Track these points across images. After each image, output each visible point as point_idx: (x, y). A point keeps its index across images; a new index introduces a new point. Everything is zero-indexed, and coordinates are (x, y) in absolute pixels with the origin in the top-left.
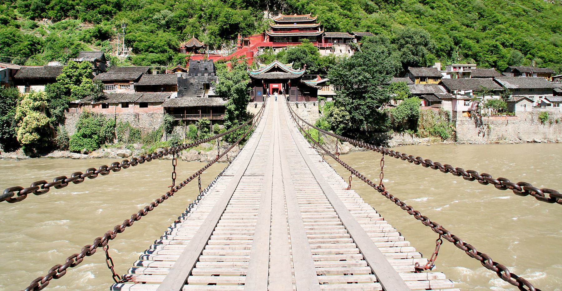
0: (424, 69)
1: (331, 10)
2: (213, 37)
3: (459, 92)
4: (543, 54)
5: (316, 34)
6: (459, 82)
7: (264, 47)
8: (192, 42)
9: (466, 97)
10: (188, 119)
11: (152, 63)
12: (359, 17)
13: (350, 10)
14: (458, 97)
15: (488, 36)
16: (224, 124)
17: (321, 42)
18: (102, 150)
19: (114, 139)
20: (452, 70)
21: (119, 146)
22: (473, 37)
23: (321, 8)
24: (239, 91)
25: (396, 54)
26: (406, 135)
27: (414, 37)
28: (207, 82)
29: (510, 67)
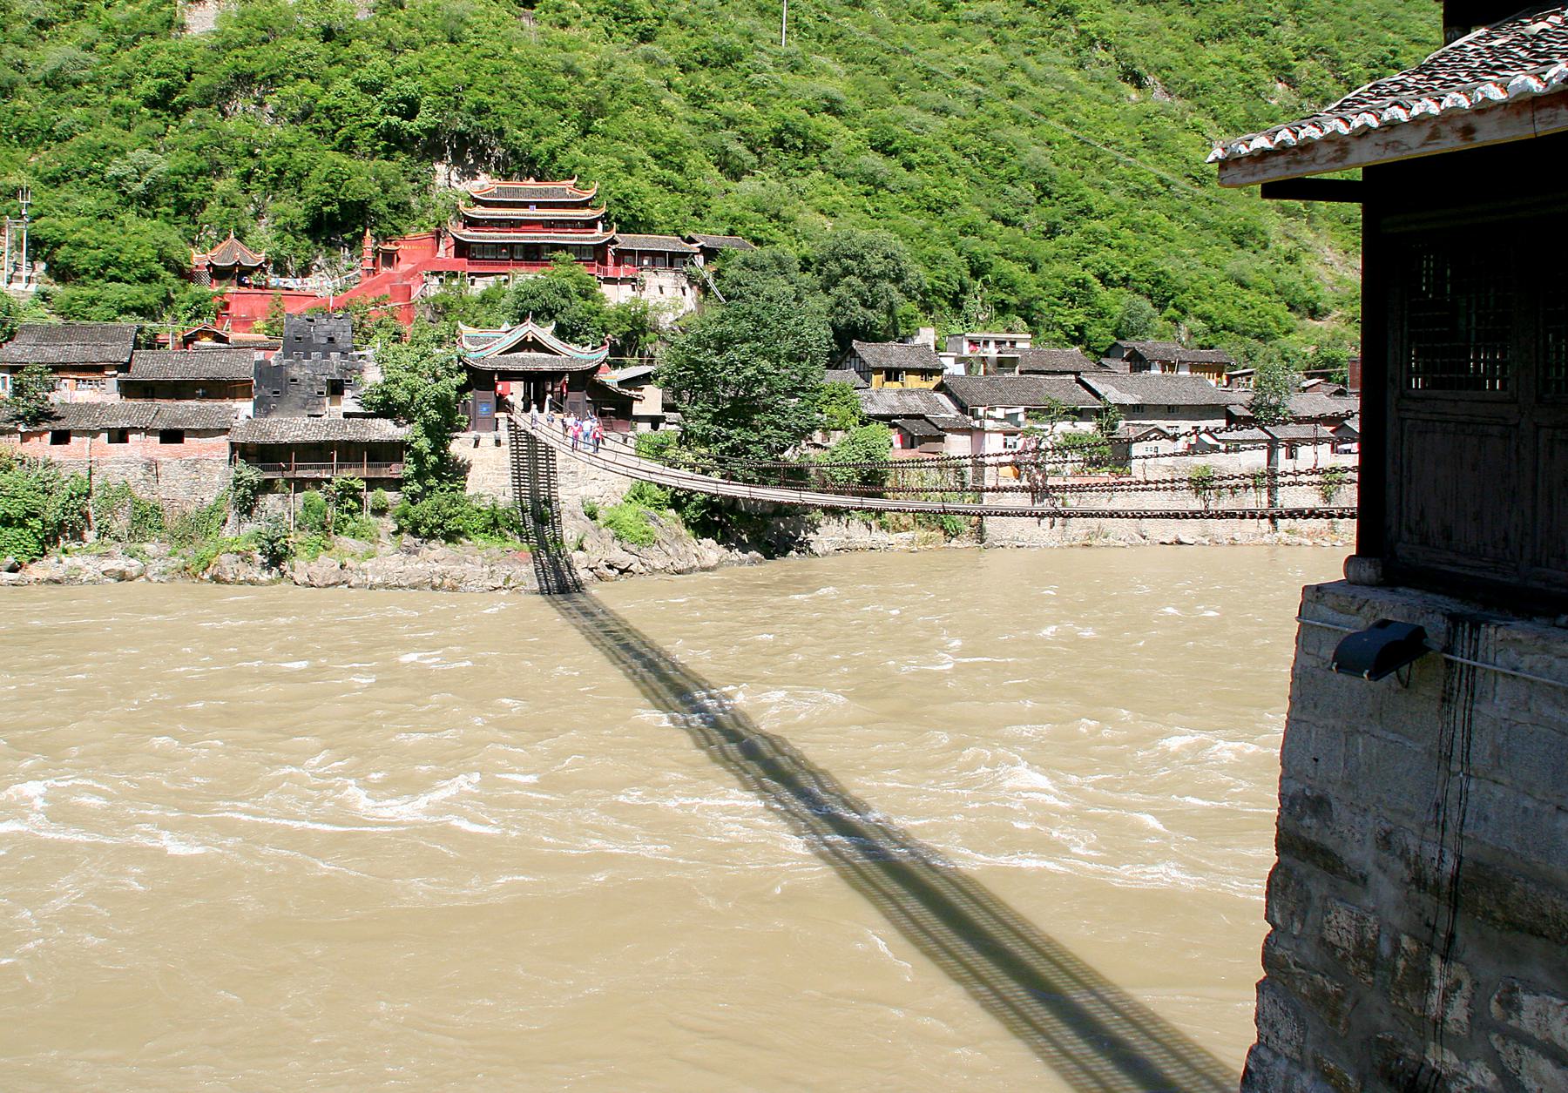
0: (893, 346)
1: (629, 169)
2: (289, 237)
3: (991, 413)
4: (1208, 307)
5: (594, 239)
6: (990, 384)
7: (441, 273)
8: (229, 253)
9: (1008, 426)
10: (300, 474)
11: (120, 312)
12: (707, 189)
13: (680, 169)
14: (989, 424)
15: (1063, 252)
16: (403, 489)
17: (604, 262)
18: (54, 560)
19: (86, 531)
20: (966, 350)
21: (102, 550)
22: (1020, 254)
23: (602, 161)
24: (442, 404)
25: (819, 303)
26: (855, 523)
27: (868, 257)
28: (338, 377)
29: (1120, 342)
